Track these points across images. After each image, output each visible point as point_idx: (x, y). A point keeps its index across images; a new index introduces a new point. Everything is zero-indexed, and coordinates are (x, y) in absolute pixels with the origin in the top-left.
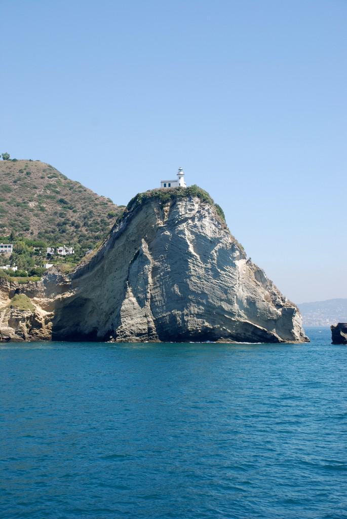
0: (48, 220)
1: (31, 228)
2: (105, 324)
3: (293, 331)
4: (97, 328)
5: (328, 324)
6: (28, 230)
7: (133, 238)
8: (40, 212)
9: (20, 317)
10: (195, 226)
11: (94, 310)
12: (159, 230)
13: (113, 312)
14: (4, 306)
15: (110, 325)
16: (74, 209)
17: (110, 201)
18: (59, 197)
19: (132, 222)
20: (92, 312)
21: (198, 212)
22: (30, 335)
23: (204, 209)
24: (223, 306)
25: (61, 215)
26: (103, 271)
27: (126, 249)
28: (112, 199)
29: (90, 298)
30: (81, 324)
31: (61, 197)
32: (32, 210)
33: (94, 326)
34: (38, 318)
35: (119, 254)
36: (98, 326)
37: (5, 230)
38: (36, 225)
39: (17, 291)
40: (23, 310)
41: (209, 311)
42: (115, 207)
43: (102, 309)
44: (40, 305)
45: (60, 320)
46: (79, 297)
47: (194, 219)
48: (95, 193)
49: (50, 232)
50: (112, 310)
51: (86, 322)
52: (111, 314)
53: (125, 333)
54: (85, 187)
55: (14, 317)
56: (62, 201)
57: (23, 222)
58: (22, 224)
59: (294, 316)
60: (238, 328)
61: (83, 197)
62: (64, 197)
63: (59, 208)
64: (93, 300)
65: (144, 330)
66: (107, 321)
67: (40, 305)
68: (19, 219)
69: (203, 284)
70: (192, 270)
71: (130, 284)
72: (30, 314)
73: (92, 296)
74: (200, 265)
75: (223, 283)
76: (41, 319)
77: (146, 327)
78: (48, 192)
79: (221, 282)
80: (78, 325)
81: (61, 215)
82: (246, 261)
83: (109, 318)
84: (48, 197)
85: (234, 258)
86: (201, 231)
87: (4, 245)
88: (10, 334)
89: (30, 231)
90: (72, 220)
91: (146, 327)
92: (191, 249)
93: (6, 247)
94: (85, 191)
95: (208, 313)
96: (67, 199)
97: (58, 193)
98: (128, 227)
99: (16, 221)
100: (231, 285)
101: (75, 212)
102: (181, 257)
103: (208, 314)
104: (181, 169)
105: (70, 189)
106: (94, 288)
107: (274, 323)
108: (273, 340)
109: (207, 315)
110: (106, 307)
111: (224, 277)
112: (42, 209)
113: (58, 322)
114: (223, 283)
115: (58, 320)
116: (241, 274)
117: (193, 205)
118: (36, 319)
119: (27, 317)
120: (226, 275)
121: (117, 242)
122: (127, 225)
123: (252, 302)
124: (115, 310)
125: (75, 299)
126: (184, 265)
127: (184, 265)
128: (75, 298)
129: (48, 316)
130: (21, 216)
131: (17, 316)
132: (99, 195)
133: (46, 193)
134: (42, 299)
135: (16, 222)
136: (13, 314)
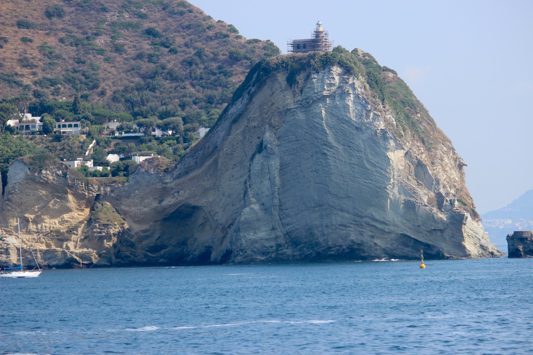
0: (129, 68)
1: (102, 85)
2: (222, 242)
3: (463, 243)
4: (211, 247)
5: (262, 234)
6: (95, 87)
7: (255, 124)
8: (114, 54)
9: (104, 234)
10: (336, 107)
11: (205, 222)
12: (288, 112)
13: (232, 224)
14: (81, 218)
15: (229, 243)
16: (172, 47)
17: (235, 31)
18: (147, 25)
19: (254, 100)
20: (203, 225)
21: (340, 87)
22: (119, 258)
23: (347, 83)
24: (374, 214)
25: (150, 58)
26: (217, 166)
27: (247, 138)
28: (237, 27)
29: (199, 205)
30: (189, 242)
31: (149, 24)
32: (101, 52)
33: (207, 244)
34: (128, 235)
35: (237, 144)
36: (211, 245)
37: (59, 89)
38: (108, 79)
39: (98, 197)
40: (108, 225)
41: (356, 221)
42: (243, 41)
43: (217, 220)
44: (130, 216)
45: (159, 237)
46: (184, 205)
47: (335, 97)
48: (208, 14)
49: (132, 89)
50: (230, 222)
51: (196, 239)
52: (229, 227)
53: (246, 252)
54: (190, 5)
55: (96, 234)
56: (150, 32)
57: (87, 74)
58: (86, 78)
59: (465, 224)
60: (393, 242)
61: (187, 23)
62: (153, 25)
63: (146, 46)
64: (205, 209)
65: (272, 247)
66: (224, 237)
67: (130, 216)
68: (81, 69)
69: (347, 185)
70: (332, 167)
71: (252, 187)
72: (117, 230)
73: (201, 202)
74: (343, 160)
75: (374, 183)
76: (133, 236)
77: (273, 243)
78: (126, 15)
79: (370, 181)
80: (184, 243)
81: (150, 58)
82: (405, 152)
83: (227, 233)
84: (128, 26)
85: (387, 149)
86: (343, 113)
87: (67, 124)
88: (92, 257)
89: (100, 89)
90: (169, 66)
91: (273, 243)
92: (331, 139)
93: (70, 126)
94: (190, 11)
95: (354, 223)
96: (159, 27)
97: (142, 16)
98: (248, 107)
99: (75, 71)
100: (383, 186)
101: (173, 51)
102: (318, 150)
103: (354, 224)
104: (320, 23)
105: (164, 9)
106: (206, 191)
107: (439, 233)
108: (439, 256)
109: (352, 226)
110: (221, 217)
111: (374, 175)
112: (118, 49)
113: (157, 239)
114: (374, 183)
115: (157, 238)
116: (396, 169)
117: (333, 78)
118: (126, 236)
119: (113, 234)
120: (377, 172)
121: (234, 126)
122: (247, 104)
123: (410, 206)
124: (234, 221)
125: (180, 207)
126: (322, 160)
127: (322, 160)
128: (180, 205)
129: (144, 231)
130: (84, 63)
131: (101, 233)
132: (216, 18)
133: (124, 17)
134: (133, 208)
135: (75, 75)
136: (95, 230)
